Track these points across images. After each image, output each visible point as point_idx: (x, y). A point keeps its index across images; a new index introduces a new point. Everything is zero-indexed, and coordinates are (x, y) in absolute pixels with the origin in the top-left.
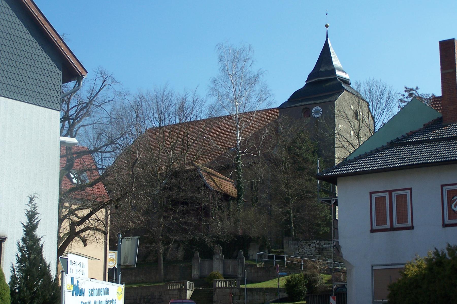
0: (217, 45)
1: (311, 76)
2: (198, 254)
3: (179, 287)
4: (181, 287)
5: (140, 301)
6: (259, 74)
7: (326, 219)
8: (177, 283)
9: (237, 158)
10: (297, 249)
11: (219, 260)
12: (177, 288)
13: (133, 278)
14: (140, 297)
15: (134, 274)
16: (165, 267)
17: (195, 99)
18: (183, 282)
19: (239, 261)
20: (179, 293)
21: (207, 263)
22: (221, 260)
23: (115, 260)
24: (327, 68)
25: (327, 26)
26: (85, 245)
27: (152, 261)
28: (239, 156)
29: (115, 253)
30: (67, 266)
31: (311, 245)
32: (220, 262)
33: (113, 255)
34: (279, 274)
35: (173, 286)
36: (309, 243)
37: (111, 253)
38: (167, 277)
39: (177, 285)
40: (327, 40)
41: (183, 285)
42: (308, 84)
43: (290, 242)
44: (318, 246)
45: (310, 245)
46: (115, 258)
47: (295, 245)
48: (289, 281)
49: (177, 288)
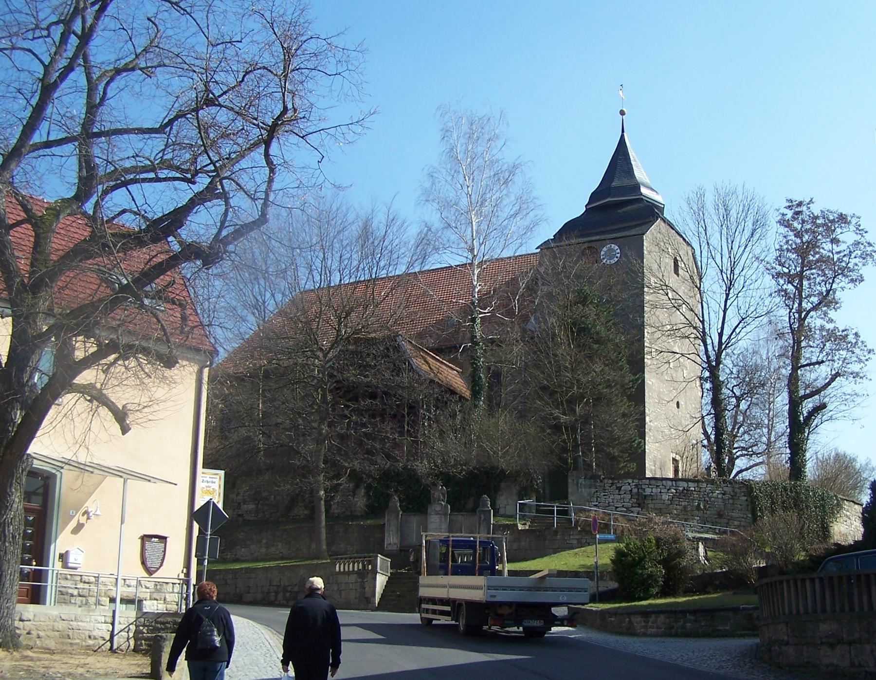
0: (439, 108)
1: (594, 196)
2: (396, 502)
3: (361, 567)
4: (364, 566)
5: (276, 597)
6: (515, 167)
7: (631, 446)
8: (354, 560)
9: (473, 320)
10: (595, 496)
11: (439, 514)
12: (356, 569)
13: (263, 550)
14: (275, 588)
15: (264, 541)
16: (329, 527)
17: (391, 217)
18: (370, 557)
19: (481, 518)
20: (359, 580)
21: (414, 520)
22: (445, 514)
23: (217, 492)
24: (626, 182)
25: (622, 113)
26: (125, 430)
27: (302, 517)
28: (475, 318)
29: (218, 477)
30: (352, 644)
31: (622, 488)
32: (443, 520)
33: (214, 480)
34: (598, 536)
35: (346, 566)
36: (618, 485)
37: (208, 476)
38: (333, 548)
39: (356, 564)
40: (622, 136)
41: (369, 562)
42: (590, 210)
43: (580, 481)
44: (635, 490)
45: (619, 489)
46: (217, 488)
47: (590, 488)
48: (619, 553)
49: (356, 569)
